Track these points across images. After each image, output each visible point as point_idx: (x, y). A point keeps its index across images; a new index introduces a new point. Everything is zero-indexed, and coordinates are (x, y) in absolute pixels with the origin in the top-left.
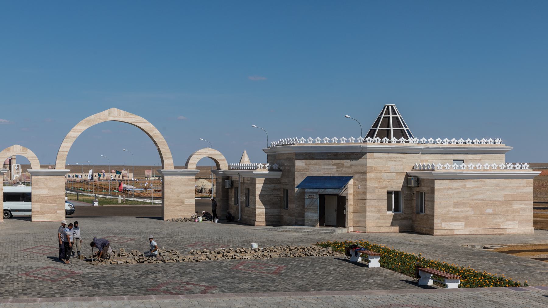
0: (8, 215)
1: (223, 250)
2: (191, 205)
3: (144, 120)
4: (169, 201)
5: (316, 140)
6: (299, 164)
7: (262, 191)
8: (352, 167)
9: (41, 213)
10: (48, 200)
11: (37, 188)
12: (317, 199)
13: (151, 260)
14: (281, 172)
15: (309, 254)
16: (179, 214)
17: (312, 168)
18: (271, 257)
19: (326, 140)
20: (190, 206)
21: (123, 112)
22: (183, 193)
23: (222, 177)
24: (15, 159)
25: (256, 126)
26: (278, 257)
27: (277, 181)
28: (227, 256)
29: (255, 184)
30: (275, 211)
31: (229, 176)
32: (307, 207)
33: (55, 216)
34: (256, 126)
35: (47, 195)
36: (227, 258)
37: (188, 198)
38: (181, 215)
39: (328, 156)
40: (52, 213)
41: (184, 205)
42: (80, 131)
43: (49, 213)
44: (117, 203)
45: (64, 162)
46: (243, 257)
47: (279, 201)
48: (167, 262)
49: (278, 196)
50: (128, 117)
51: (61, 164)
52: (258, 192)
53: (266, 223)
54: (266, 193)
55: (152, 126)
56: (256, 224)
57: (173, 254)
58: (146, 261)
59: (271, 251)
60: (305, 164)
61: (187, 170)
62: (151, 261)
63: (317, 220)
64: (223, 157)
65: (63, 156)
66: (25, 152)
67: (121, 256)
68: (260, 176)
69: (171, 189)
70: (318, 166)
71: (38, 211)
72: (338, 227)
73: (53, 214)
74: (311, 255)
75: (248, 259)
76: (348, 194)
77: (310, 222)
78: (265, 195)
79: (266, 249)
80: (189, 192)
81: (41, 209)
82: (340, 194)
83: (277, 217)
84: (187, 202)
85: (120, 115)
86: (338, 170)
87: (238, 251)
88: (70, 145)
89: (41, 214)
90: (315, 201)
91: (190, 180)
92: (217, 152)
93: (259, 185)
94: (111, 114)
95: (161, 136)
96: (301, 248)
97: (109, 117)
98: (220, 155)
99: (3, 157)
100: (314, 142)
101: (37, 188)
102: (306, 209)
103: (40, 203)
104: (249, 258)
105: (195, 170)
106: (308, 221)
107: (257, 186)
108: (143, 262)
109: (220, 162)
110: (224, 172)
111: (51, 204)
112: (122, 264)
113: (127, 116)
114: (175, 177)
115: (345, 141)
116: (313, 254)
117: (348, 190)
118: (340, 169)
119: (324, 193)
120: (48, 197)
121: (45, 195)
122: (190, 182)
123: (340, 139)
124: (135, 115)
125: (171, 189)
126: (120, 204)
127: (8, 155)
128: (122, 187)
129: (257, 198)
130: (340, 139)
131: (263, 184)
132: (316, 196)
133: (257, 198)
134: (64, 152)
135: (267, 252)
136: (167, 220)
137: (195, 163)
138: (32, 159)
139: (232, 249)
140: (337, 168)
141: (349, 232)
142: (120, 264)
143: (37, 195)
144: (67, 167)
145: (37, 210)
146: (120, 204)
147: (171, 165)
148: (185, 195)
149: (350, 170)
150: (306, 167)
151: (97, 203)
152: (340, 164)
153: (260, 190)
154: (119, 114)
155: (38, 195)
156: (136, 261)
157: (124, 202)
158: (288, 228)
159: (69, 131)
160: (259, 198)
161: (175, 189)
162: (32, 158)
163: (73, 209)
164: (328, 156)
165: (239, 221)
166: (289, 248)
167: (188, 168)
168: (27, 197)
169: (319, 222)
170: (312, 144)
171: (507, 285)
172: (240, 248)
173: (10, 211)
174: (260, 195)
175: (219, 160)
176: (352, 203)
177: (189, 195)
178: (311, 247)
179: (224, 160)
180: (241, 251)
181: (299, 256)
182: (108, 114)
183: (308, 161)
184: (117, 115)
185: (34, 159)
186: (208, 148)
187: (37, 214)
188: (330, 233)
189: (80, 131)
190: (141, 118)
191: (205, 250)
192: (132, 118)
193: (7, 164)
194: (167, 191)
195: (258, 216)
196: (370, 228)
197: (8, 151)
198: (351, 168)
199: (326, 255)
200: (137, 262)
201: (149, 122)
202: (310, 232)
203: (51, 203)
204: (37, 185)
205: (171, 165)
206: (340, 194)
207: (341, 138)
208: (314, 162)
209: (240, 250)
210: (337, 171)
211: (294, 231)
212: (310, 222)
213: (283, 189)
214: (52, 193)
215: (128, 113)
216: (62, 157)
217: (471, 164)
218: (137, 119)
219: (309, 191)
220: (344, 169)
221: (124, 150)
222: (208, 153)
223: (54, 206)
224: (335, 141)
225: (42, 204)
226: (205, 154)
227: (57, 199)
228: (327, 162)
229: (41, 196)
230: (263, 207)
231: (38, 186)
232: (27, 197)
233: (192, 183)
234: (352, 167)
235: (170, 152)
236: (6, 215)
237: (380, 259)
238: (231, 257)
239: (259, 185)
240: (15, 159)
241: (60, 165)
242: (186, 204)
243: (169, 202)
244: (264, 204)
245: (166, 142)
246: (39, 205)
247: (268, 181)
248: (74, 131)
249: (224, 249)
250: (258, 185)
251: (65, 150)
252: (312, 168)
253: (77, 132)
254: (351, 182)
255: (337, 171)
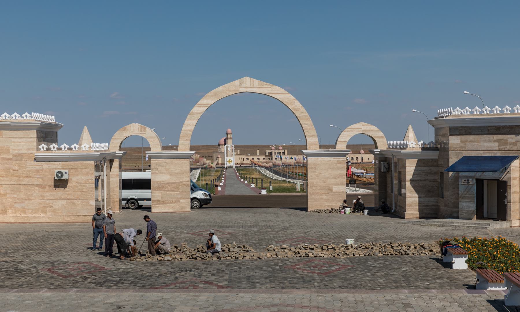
0: (134, 205)
1: (306, 247)
2: (341, 193)
3: (283, 91)
4: (314, 188)
5: (474, 110)
6: (454, 141)
7: (414, 175)
8: (518, 143)
9: (163, 203)
10: (169, 187)
11: (157, 174)
12: (473, 185)
13: (205, 256)
14: (438, 152)
15: (403, 253)
16: (327, 204)
17: (469, 146)
18: (354, 255)
19: (487, 110)
20: (340, 194)
21: (256, 82)
22: (332, 179)
23: (379, 158)
24: (231, 138)
25: (468, 93)
26: (363, 255)
27: (434, 163)
28: (299, 253)
29: (404, 167)
30: (432, 201)
31: (387, 156)
32: (462, 195)
33: (178, 206)
34: (468, 93)
35: (169, 181)
36: (298, 255)
37: (338, 184)
38: (328, 206)
39: (488, 130)
40: (174, 203)
41: (332, 194)
42: (206, 105)
43: (171, 202)
44: (294, 190)
45: (188, 142)
46: (318, 254)
47: (436, 188)
48: (222, 259)
49: (435, 182)
50: (262, 88)
51: (184, 145)
52: (409, 176)
53: (419, 215)
54: (418, 178)
55: (292, 97)
56: (407, 216)
57: (245, 251)
58: (200, 257)
59: (367, 248)
60: (461, 142)
61: (177, 151)
62: (205, 257)
63: (474, 211)
64: (381, 134)
65: (186, 136)
66: (143, 131)
67: (182, 252)
68: (411, 157)
69: (316, 173)
70: (476, 143)
71: (159, 201)
72: (498, 221)
73: (175, 204)
74: (405, 254)
75: (324, 257)
76: (511, 178)
77: (465, 214)
78: (417, 180)
79: (361, 246)
80: (338, 178)
81: (162, 198)
82: (501, 179)
83: (434, 207)
84: (335, 189)
85: (253, 86)
86: (500, 148)
87: (325, 247)
88: (195, 122)
89: (162, 204)
90: (471, 188)
91: (339, 162)
92: (374, 128)
93: (410, 168)
94: (243, 84)
95: (303, 110)
96: (406, 245)
97: (240, 88)
98: (378, 131)
99: (119, 137)
100: (472, 113)
101: (157, 174)
102: (461, 197)
103: (161, 191)
104: (325, 256)
105: (345, 150)
106: (463, 212)
107: (408, 169)
108: (196, 259)
109: (377, 140)
110: (381, 153)
111: (174, 192)
112: (169, 260)
113: (262, 87)
114: (320, 159)
115: (510, 111)
116: (408, 252)
117: (511, 173)
118: (503, 147)
119: (481, 178)
120: (170, 184)
121: (166, 182)
122: (338, 165)
123: (493, 109)
124: (272, 85)
125: (316, 173)
126: (299, 192)
127: (124, 135)
128: (350, 171)
129: (408, 184)
130: (493, 109)
131: (416, 166)
132: (472, 181)
133: (408, 184)
134: (188, 131)
135: (361, 249)
136: (310, 212)
137: (345, 141)
138: (151, 139)
139: (318, 245)
140: (499, 145)
141: (512, 227)
142: (167, 260)
143: (157, 182)
144: (192, 148)
145: (158, 199)
146: (299, 192)
147: (315, 145)
148: (333, 181)
149: (515, 148)
150: (462, 145)
151: (265, 191)
152: (503, 140)
153: (411, 174)
154: (252, 84)
155: (159, 181)
156: (188, 257)
157: (305, 190)
158: (434, 222)
159: (193, 106)
160: (410, 184)
161: (320, 174)
162: (152, 138)
163: (209, 198)
164: (488, 130)
165: (393, 212)
166: (391, 244)
167: (337, 147)
168: (145, 184)
169: (476, 214)
170: (468, 115)
171: (453, 288)
172: (327, 245)
173: (137, 200)
174: (412, 181)
175: (376, 137)
176: (518, 190)
177: (338, 180)
178: (419, 244)
179: (382, 137)
180: (328, 247)
181: (391, 254)
182: (239, 84)
183: (464, 137)
184: (249, 86)
185: (154, 140)
186: (361, 122)
187: (158, 204)
188: (483, 228)
189: (206, 105)
190: (279, 88)
191: (284, 246)
192: (268, 88)
193: (222, 145)
194: (311, 176)
195: (409, 206)
196: (52, 215)
197: (124, 130)
198: (516, 145)
199: (425, 253)
200: (190, 258)
201: (288, 93)
202: (459, 226)
203: (173, 191)
204: (157, 169)
205: (315, 145)
206: (501, 179)
207: (505, 107)
208: (471, 138)
209: (327, 246)
210: (500, 149)
211: (440, 225)
212: (466, 214)
213: (440, 172)
214: (175, 179)
215: (263, 83)
216: (186, 137)
217: (43, 145)
218: (274, 90)
219: (463, 174)
220: (508, 147)
221: (331, 125)
222: (361, 129)
223: (177, 194)
224: (497, 111)
225: (163, 192)
226: (357, 130)
227: (180, 186)
228: (488, 139)
229: (162, 182)
230: (416, 195)
231: (159, 171)
232: (145, 184)
233: (341, 165)
234: (518, 143)
235: (314, 128)
236: (133, 205)
237: (467, 258)
238: (305, 255)
239: (410, 168)
240: (231, 138)
241: (184, 147)
242: (334, 192)
243: (314, 190)
244: (417, 191)
245: (309, 117)
246: (159, 193)
247: (421, 163)
248: (199, 105)
249: (307, 246)
250: (409, 167)
251: (189, 128)
252: (469, 146)
253: (203, 107)
254: (515, 164)
255: (499, 150)
